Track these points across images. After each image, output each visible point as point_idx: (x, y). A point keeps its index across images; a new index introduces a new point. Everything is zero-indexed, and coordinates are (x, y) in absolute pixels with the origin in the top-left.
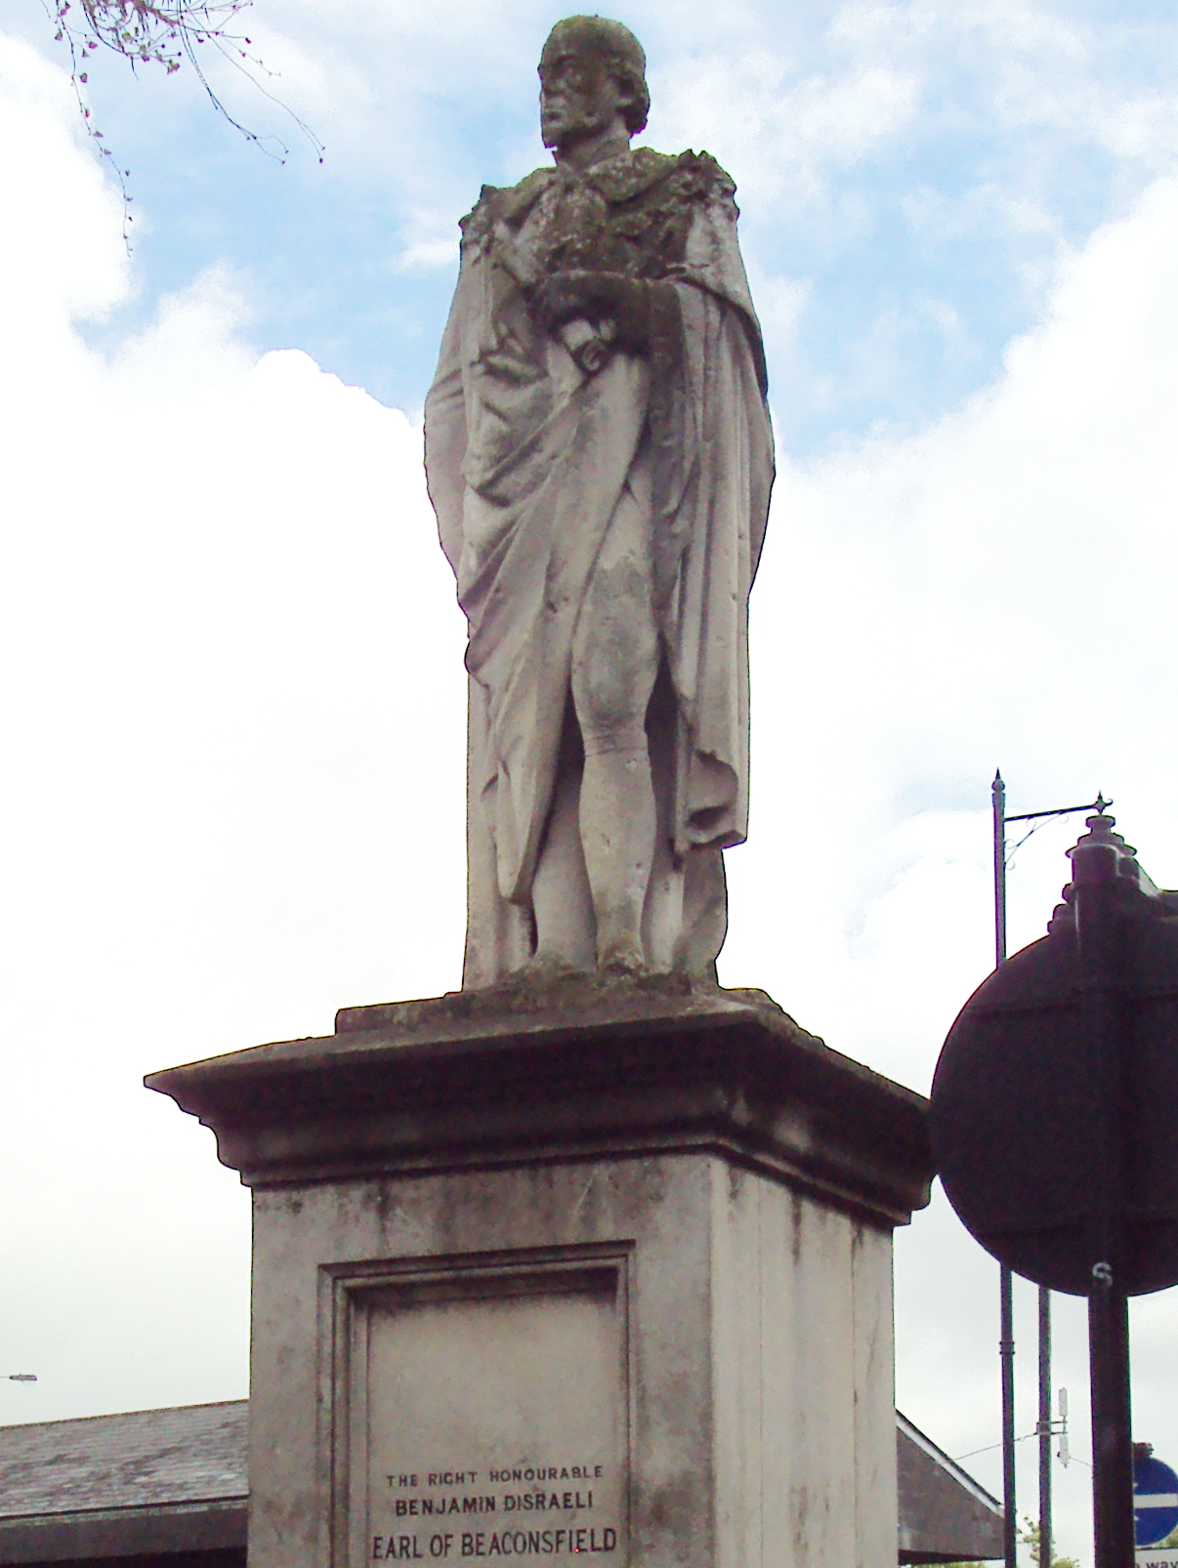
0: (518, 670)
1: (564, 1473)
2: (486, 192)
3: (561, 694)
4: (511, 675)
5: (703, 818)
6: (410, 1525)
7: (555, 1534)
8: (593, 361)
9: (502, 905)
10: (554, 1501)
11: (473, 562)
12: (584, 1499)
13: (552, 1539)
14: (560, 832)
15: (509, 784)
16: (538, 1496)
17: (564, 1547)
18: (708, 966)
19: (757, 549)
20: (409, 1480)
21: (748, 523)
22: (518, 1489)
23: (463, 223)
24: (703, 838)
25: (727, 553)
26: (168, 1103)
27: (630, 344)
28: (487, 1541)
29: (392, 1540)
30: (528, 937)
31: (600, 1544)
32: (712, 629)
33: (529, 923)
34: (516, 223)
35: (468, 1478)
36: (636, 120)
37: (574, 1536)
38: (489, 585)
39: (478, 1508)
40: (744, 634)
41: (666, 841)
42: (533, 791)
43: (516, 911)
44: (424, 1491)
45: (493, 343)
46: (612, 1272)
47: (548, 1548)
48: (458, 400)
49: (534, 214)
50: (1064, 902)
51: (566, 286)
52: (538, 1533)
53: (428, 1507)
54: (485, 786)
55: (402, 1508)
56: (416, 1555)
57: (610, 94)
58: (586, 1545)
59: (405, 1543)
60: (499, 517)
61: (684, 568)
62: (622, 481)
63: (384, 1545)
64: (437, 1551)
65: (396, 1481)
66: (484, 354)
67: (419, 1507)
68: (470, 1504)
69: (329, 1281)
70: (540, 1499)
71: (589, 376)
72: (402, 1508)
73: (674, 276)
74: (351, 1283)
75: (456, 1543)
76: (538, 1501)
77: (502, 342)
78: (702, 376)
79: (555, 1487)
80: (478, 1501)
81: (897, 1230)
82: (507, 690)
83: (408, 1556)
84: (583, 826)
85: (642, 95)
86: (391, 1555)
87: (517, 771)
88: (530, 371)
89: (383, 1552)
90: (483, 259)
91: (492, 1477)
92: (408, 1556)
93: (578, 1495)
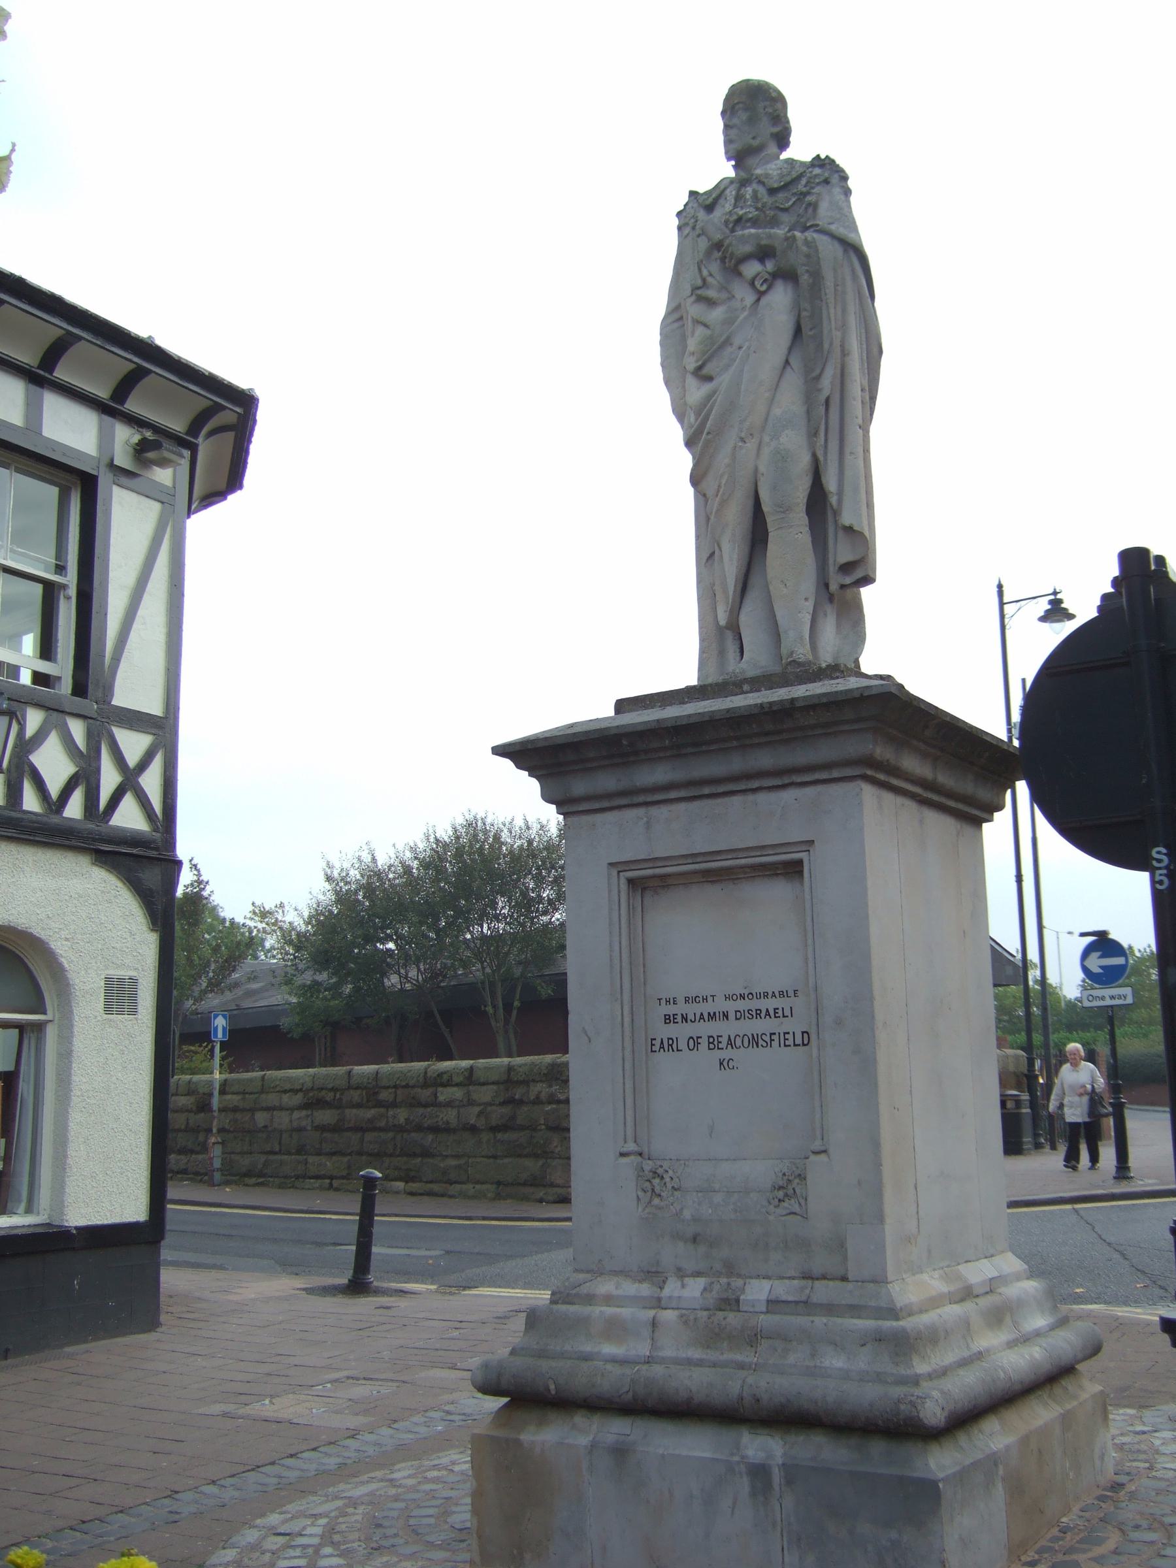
0: (724, 482)
1: (774, 995)
2: (693, 194)
3: (752, 493)
4: (719, 486)
5: (847, 568)
6: (672, 1031)
7: (768, 1035)
8: (762, 285)
9: (720, 630)
10: (774, 995)
11: (692, 419)
12: (787, 1012)
13: (767, 1039)
14: (755, 580)
15: (721, 556)
16: (756, 1010)
17: (775, 1044)
18: (854, 662)
19: (873, 399)
20: (672, 1001)
21: (867, 381)
22: (742, 1005)
23: (679, 214)
24: (848, 580)
25: (854, 399)
26: (507, 764)
27: (787, 275)
28: (724, 1040)
29: (662, 1039)
30: (738, 650)
31: (799, 1041)
32: (847, 450)
33: (739, 642)
34: (710, 208)
35: (710, 999)
36: (782, 139)
37: (782, 1035)
38: (702, 433)
39: (717, 1019)
40: (866, 451)
41: (823, 585)
42: (735, 556)
43: (729, 635)
44: (681, 1008)
45: (699, 282)
46: (800, 863)
47: (765, 1044)
48: (680, 323)
49: (721, 201)
50: (1112, 590)
51: (743, 240)
52: (757, 1035)
53: (685, 1019)
54: (707, 557)
55: (668, 1019)
56: (678, 1050)
57: (767, 129)
58: (790, 1042)
59: (671, 1042)
60: (707, 387)
61: (827, 410)
62: (785, 358)
63: (657, 1043)
64: (691, 1047)
65: (663, 1002)
66: (695, 289)
67: (679, 1018)
68: (712, 1016)
69: (615, 873)
70: (758, 1012)
71: (761, 294)
72: (668, 1019)
73: (812, 230)
74: (630, 874)
75: (704, 1042)
76: (757, 1014)
77: (704, 280)
78: (833, 290)
79: (770, 1004)
80: (717, 1014)
81: (984, 825)
82: (717, 495)
83: (673, 1051)
84: (769, 576)
85: (787, 125)
86: (662, 1050)
87: (726, 546)
88: (724, 295)
89: (656, 1048)
90: (691, 234)
91: (726, 998)
92: (673, 1051)
93: (783, 1009)
